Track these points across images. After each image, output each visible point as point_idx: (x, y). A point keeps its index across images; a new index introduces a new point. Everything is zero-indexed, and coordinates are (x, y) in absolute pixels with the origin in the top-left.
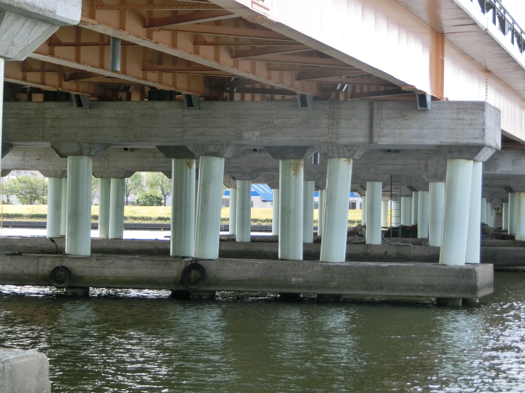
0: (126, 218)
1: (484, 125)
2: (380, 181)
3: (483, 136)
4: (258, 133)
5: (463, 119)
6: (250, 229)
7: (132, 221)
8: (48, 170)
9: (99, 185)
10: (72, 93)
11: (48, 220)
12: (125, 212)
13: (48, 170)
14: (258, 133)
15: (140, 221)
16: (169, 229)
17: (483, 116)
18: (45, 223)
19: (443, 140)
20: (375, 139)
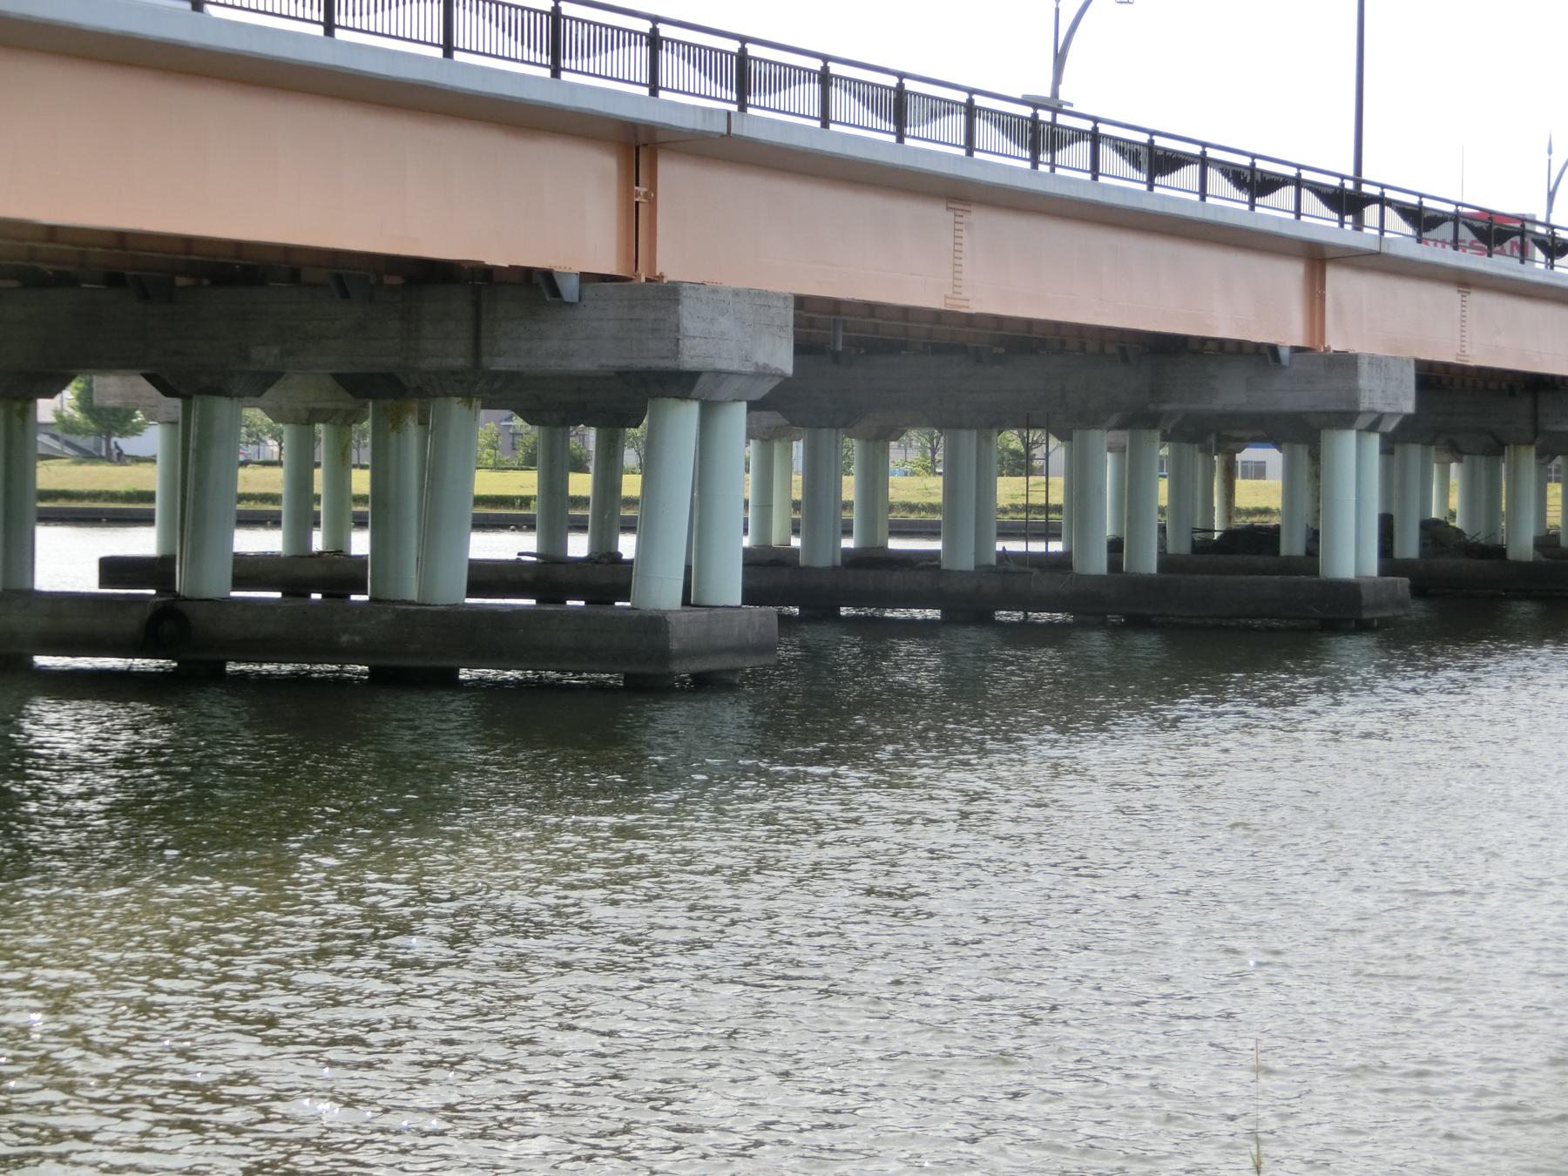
0: (891, 508)
1: (678, 330)
2: (970, 428)
3: (676, 353)
4: (276, 350)
5: (638, 320)
6: (234, 520)
7: (903, 514)
8: (281, 408)
9: (368, 440)
10: (127, 273)
11: (283, 508)
12: (1237, 499)
13: (281, 408)
14: (276, 350)
15: (923, 513)
16: (146, 519)
17: (676, 312)
18: (152, 512)
19: (604, 361)
20: (485, 360)
